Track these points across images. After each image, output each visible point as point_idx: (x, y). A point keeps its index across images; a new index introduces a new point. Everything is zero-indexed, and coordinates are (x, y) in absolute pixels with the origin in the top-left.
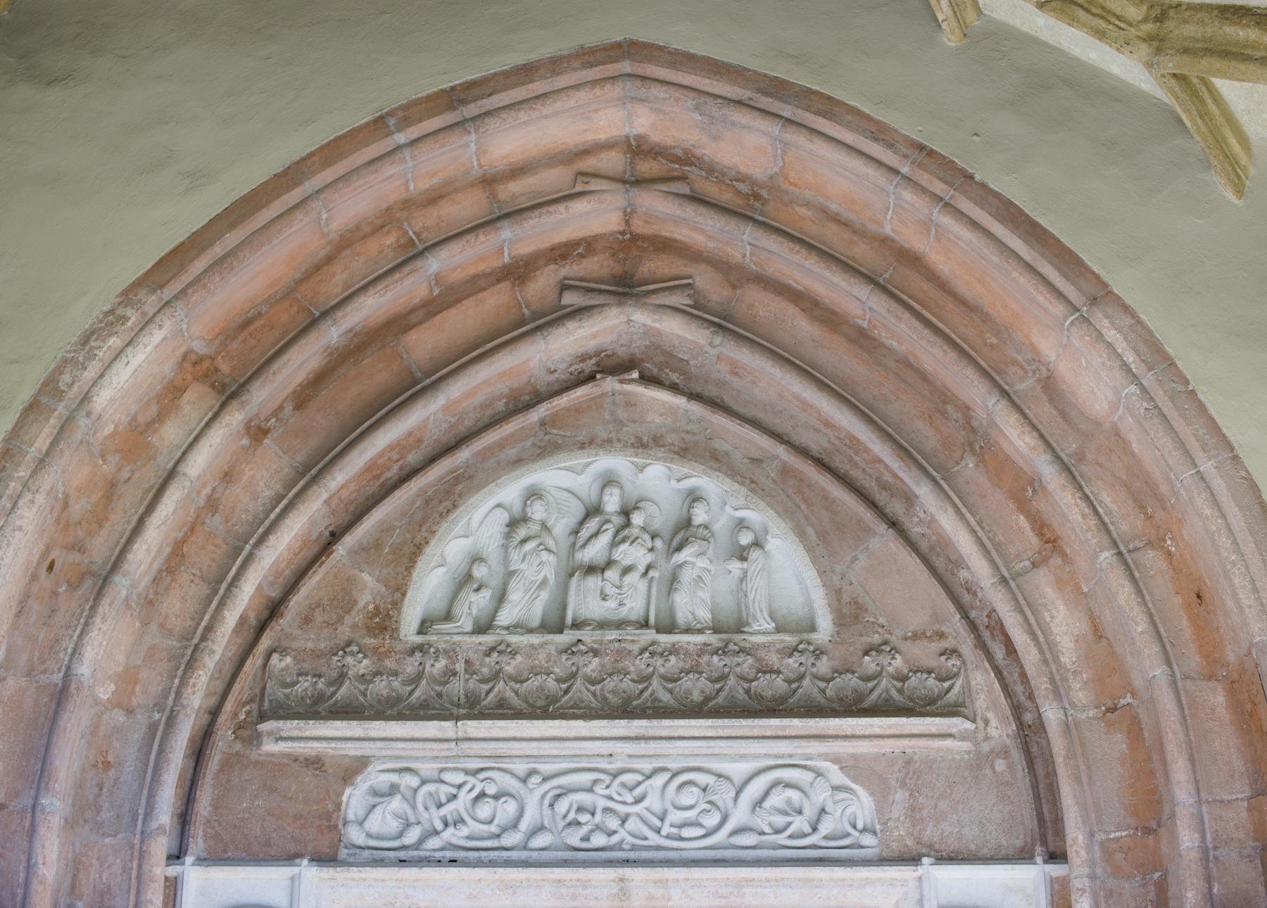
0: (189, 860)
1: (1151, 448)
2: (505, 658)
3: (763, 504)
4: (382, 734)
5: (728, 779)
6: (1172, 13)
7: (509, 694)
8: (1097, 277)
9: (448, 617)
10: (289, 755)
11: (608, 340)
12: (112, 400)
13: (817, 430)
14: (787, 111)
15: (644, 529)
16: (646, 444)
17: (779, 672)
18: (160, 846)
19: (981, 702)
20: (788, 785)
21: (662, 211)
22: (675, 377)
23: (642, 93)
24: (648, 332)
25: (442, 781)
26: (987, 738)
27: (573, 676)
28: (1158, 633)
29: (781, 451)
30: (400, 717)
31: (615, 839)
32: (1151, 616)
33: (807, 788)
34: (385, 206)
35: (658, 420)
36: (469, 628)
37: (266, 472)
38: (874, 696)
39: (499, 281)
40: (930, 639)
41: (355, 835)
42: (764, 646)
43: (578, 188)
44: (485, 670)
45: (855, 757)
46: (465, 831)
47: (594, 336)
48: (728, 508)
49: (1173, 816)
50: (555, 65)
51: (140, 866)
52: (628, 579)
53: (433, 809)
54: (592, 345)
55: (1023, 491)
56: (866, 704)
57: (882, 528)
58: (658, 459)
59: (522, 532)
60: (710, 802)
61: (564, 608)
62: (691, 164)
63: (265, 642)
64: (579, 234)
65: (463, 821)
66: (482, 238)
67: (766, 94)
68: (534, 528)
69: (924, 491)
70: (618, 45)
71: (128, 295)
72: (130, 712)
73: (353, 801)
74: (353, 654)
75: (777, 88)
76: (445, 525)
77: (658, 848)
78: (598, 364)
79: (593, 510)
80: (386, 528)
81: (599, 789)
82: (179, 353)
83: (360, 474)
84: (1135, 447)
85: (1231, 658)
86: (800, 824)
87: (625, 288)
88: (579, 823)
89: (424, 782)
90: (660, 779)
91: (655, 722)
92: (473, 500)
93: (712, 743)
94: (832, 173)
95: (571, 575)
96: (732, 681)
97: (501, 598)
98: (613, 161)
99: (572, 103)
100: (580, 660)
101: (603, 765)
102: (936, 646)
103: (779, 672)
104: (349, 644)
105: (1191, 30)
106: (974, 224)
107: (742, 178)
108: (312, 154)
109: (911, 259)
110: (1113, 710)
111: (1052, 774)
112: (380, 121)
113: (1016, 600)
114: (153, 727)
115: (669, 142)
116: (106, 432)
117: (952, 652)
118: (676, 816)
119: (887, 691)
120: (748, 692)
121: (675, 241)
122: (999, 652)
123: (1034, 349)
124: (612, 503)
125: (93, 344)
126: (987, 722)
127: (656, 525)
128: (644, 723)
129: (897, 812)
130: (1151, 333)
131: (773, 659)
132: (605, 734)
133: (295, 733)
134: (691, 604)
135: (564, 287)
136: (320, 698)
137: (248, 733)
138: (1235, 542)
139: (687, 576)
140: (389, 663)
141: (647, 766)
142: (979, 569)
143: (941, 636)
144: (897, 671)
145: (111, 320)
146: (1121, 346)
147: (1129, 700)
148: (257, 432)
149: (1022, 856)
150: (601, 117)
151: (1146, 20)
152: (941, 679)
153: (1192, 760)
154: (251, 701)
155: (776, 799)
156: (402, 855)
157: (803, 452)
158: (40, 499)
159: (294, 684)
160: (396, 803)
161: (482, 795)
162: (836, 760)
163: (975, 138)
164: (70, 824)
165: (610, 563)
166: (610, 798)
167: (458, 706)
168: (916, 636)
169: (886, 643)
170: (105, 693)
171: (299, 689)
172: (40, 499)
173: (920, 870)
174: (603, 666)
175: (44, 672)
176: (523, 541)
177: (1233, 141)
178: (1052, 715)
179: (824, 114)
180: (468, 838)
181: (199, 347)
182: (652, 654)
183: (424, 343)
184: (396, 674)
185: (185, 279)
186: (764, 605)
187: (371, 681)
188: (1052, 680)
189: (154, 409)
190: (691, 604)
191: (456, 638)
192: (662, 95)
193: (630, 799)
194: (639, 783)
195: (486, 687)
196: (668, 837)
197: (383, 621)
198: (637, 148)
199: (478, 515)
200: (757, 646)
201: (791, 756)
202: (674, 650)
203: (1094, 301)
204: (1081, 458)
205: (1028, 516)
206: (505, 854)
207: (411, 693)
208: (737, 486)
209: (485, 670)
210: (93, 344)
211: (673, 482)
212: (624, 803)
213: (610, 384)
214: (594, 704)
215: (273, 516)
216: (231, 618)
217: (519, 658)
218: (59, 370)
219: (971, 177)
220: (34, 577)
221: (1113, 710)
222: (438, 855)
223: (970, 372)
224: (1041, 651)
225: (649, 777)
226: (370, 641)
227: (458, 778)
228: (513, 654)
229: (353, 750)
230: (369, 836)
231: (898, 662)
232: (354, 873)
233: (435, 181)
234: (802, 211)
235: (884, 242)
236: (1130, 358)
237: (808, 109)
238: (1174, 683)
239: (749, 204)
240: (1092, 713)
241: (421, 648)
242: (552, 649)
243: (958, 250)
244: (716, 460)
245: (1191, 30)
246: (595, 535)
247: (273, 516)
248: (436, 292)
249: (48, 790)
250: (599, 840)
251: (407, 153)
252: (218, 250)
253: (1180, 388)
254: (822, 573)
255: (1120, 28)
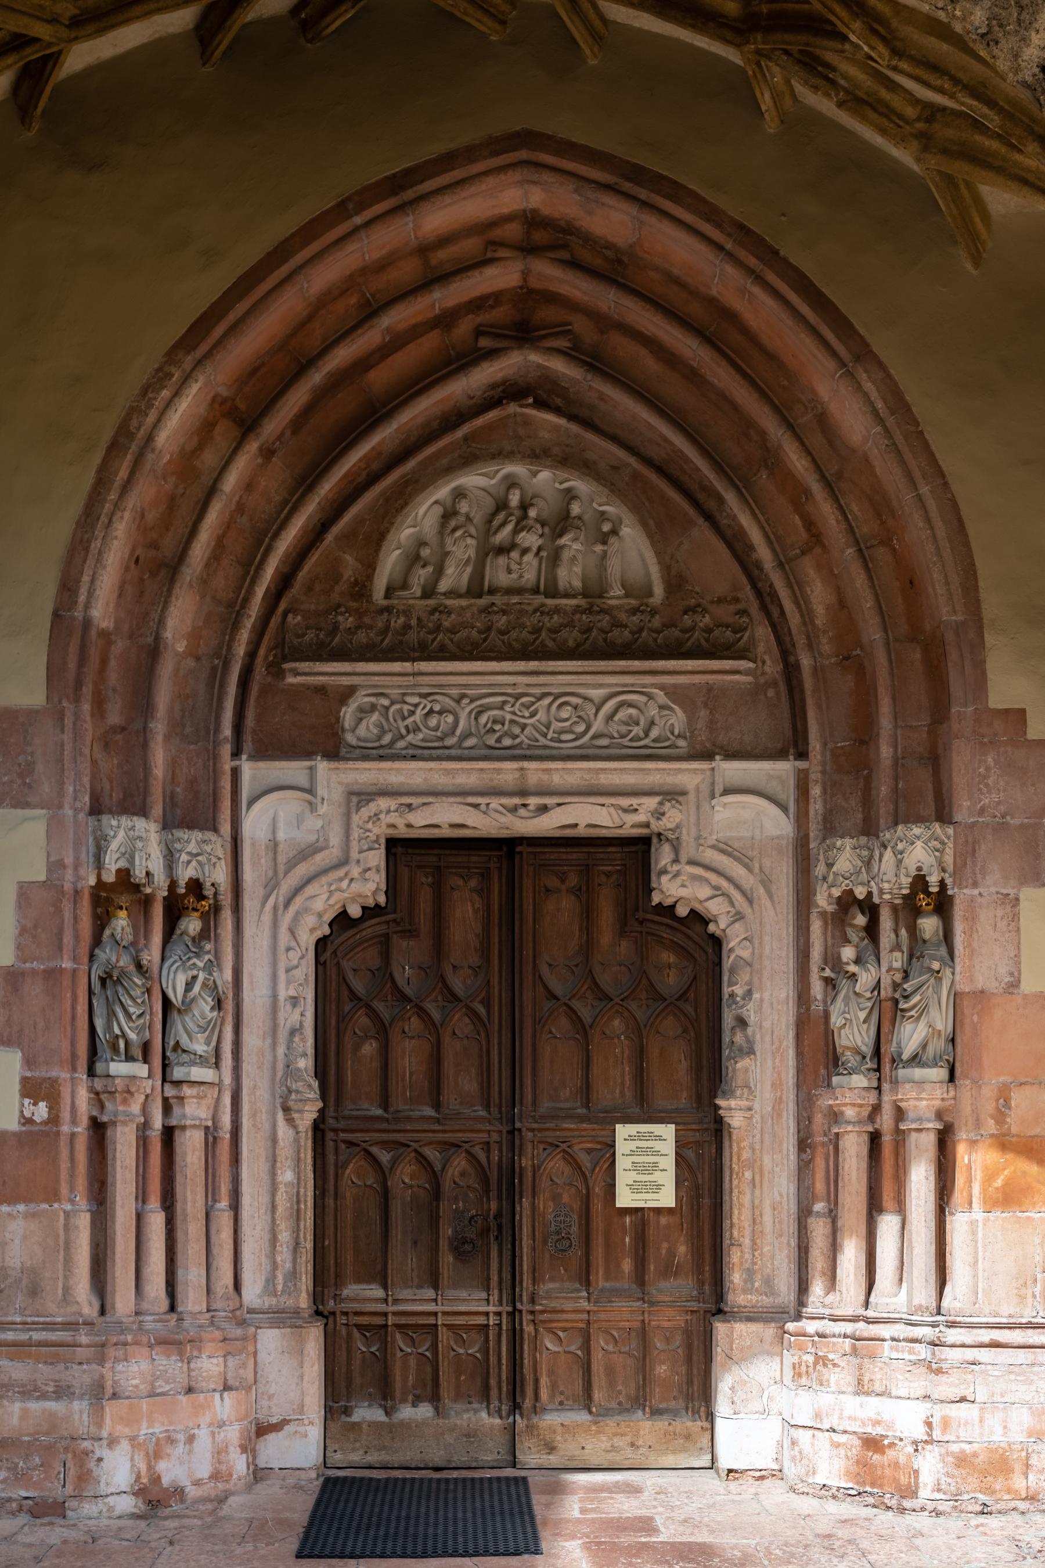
0: (244, 757)
1: (888, 472)
2: (444, 617)
3: (619, 502)
4: (364, 670)
5: (591, 700)
6: (939, 116)
7: (447, 641)
8: (862, 338)
9: (405, 586)
10: (303, 685)
11: (511, 372)
12: (168, 438)
13: (658, 444)
14: (643, 194)
15: (536, 520)
16: (538, 455)
17: (626, 626)
18: (226, 750)
19: (761, 648)
20: (631, 705)
21: (550, 274)
22: (558, 401)
23: (536, 177)
24: (539, 366)
25: (405, 702)
26: (764, 673)
27: (489, 629)
28: (880, 608)
29: (632, 461)
30: (376, 659)
31: (518, 741)
32: (876, 595)
33: (642, 706)
34: (348, 273)
35: (547, 436)
36: (419, 594)
37: (275, 480)
38: (689, 644)
39: (432, 329)
40: (729, 603)
41: (350, 738)
42: (618, 607)
43: (489, 255)
44: (430, 625)
45: (674, 686)
46: (421, 736)
47: (501, 370)
48: (595, 505)
49: (878, 734)
50: (470, 153)
51: (215, 764)
52: (526, 558)
53: (400, 722)
54: (499, 376)
55: (799, 497)
56: (683, 650)
57: (700, 521)
58: (546, 467)
59: (453, 523)
60: (579, 717)
61: (482, 578)
62: (571, 234)
63: (283, 606)
64: (489, 290)
65: (419, 730)
66: (419, 299)
67: (628, 179)
68: (462, 519)
69: (730, 497)
70: (517, 134)
71: (172, 355)
72: (198, 659)
73: (348, 716)
74: (342, 614)
75: (637, 174)
76: (400, 518)
77: (545, 747)
78: (503, 391)
79: (501, 505)
80: (359, 521)
81: (508, 708)
82: (209, 397)
83: (340, 480)
84: (878, 471)
85: (928, 628)
86: (637, 730)
87: (523, 333)
88: (494, 731)
89: (393, 703)
90: (547, 701)
91: (543, 663)
92: (418, 499)
93: (581, 677)
94: (676, 247)
95: (487, 555)
96: (595, 632)
97: (439, 572)
98: (513, 231)
99: (484, 187)
100: (495, 618)
101: (510, 691)
102: (733, 608)
103: (626, 626)
104: (339, 606)
105: (950, 133)
106: (776, 294)
107: (610, 246)
108: (293, 235)
109: (730, 316)
110: (847, 658)
111: (803, 700)
112: (342, 205)
113: (788, 578)
114: (214, 669)
115: (556, 215)
116: (165, 460)
117: (743, 612)
118: (556, 725)
119: (698, 640)
120: (605, 640)
121: (559, 294)
122: (776, 613)
123: (814, 391)
124: (514, 499)
125: (150, 395)
126: (764, 662)
127: (545, 514)
128: (536, 663)
129: (701, 724)
130: (896, 384)
131: (623, 617)
132: (510, 669)
133: (307, 670)
134: (569, 576)
135: (479, 332)
136: (321, 645)
137: (276, 670)
138: (937, 548)
139: (566, 555)
140: (367, 620)
141: (537, 691)
142: (764, 553)
143: (737, 600)
144: (706, 626)
145: (160, 377)
146: (874, 395)
147: (858, 652)
148: (267, 453)
149: (780, 755)
150: (503, 196)
151: (918, 119)
152: (735, 632)
153: (894, 699)
154: (275, 647)
155: (621, 715)
156: (381, 752)
157: (648, 461)
158: (127, 515)
159: (304, 635)
160: (375, 717)
161: (431, 711)
162: (662, 687)
163: (783, 218)
164: (167, 738)
165: (513, 546)
166: (514, 713)
167: (414, 650)
168: (720, 601)
169: (699, 605)
170: (181, 647)
171: (307, 638)
172: (127, 515)
173: (714, 764)
174: (509, 622)
175: (141, 636)
176: (454, 530)
177: (977, 220)
178: (806, 661)
179: (668, 197)
180: (423, 740)
181: (224, 392)
182: (542, 613)
183: (380, 378)
184: (371, 627)
185: (210, 341)
186: (618, 576)
187: (355, 633)
188: (808, 638)
189: (195, 441)
190: (569, 576)
191: (411, 602)
192: (551, 180)
193: (527, 714)
194: (533, 703)
195: (431, 637)
196: (551, 740)
197: (361, 589)
198: (532, 220)
199: (422, 510)
200: (612, 608)
201: (632, 685)
202: (557, 610)
203: (858, 359)
204: (839, 475)
205: (801, 517)
206: (447, 752)
207: (382, 641)
208: (601, 488)
209: (430, 625)
210: (150, 395)
211: (557, 485)
212: (523, 717)
213: (513, 408)
214: (504, 649)
215: (282, 516)
216: (260, 591)
217: (453, 616)
218: (128, 417)
219: (776, 253)
220: (127, 569)
221: (847, 658)
222: (404, 752)
223: (767, 409)
224: (802, 616)
225: (539, 699)
226: (353, 604)
227: (415, 700)
228: (449, 613)
229: (346, 681)
230: (359, 739)
231: (707, 619)
232: (351, 764)
233: (384, 252)
234: (653, 275)
235: (712, 302)
236: (880, 405)
237: (658, 193)
238: (887, 644)
239: (614, 267)
240: (833, 660)
241: (388, 609)
242: (475, 609)
243: (762, 312)
244: (586, 467)
245: (950, 133)
246: (503, 524)
247: (282, 516)
248: (387, 339)
249: (152, 717)
250: (507, 742)
251: (363, 234)
252: (232, 317)
253: (913, 429)
254: (658, 554)
255: (899, 126)
